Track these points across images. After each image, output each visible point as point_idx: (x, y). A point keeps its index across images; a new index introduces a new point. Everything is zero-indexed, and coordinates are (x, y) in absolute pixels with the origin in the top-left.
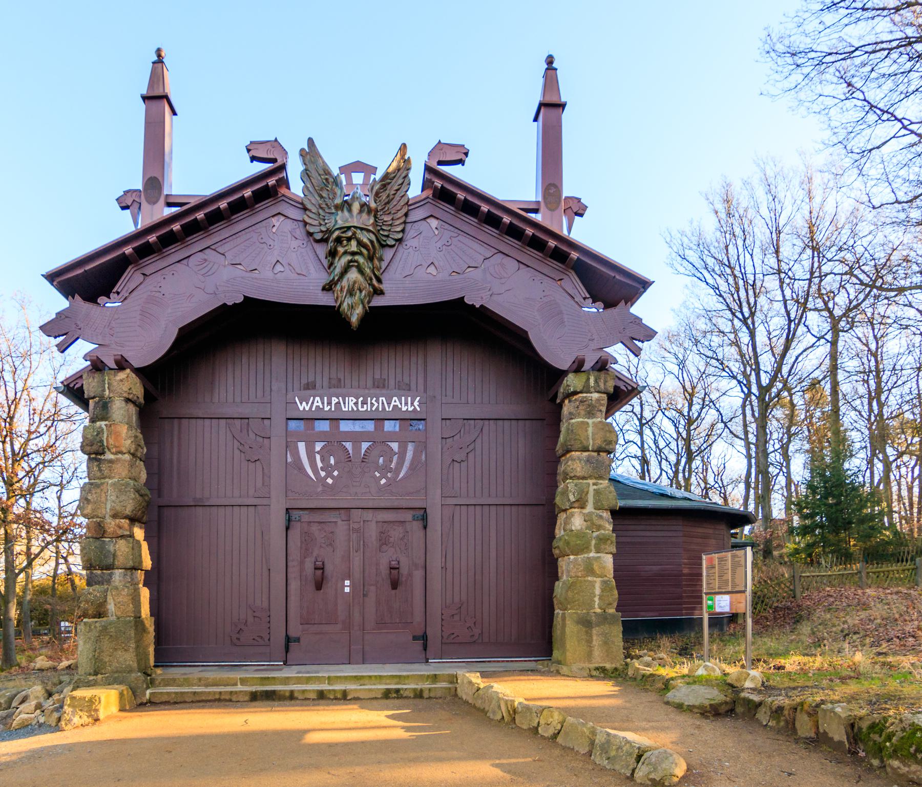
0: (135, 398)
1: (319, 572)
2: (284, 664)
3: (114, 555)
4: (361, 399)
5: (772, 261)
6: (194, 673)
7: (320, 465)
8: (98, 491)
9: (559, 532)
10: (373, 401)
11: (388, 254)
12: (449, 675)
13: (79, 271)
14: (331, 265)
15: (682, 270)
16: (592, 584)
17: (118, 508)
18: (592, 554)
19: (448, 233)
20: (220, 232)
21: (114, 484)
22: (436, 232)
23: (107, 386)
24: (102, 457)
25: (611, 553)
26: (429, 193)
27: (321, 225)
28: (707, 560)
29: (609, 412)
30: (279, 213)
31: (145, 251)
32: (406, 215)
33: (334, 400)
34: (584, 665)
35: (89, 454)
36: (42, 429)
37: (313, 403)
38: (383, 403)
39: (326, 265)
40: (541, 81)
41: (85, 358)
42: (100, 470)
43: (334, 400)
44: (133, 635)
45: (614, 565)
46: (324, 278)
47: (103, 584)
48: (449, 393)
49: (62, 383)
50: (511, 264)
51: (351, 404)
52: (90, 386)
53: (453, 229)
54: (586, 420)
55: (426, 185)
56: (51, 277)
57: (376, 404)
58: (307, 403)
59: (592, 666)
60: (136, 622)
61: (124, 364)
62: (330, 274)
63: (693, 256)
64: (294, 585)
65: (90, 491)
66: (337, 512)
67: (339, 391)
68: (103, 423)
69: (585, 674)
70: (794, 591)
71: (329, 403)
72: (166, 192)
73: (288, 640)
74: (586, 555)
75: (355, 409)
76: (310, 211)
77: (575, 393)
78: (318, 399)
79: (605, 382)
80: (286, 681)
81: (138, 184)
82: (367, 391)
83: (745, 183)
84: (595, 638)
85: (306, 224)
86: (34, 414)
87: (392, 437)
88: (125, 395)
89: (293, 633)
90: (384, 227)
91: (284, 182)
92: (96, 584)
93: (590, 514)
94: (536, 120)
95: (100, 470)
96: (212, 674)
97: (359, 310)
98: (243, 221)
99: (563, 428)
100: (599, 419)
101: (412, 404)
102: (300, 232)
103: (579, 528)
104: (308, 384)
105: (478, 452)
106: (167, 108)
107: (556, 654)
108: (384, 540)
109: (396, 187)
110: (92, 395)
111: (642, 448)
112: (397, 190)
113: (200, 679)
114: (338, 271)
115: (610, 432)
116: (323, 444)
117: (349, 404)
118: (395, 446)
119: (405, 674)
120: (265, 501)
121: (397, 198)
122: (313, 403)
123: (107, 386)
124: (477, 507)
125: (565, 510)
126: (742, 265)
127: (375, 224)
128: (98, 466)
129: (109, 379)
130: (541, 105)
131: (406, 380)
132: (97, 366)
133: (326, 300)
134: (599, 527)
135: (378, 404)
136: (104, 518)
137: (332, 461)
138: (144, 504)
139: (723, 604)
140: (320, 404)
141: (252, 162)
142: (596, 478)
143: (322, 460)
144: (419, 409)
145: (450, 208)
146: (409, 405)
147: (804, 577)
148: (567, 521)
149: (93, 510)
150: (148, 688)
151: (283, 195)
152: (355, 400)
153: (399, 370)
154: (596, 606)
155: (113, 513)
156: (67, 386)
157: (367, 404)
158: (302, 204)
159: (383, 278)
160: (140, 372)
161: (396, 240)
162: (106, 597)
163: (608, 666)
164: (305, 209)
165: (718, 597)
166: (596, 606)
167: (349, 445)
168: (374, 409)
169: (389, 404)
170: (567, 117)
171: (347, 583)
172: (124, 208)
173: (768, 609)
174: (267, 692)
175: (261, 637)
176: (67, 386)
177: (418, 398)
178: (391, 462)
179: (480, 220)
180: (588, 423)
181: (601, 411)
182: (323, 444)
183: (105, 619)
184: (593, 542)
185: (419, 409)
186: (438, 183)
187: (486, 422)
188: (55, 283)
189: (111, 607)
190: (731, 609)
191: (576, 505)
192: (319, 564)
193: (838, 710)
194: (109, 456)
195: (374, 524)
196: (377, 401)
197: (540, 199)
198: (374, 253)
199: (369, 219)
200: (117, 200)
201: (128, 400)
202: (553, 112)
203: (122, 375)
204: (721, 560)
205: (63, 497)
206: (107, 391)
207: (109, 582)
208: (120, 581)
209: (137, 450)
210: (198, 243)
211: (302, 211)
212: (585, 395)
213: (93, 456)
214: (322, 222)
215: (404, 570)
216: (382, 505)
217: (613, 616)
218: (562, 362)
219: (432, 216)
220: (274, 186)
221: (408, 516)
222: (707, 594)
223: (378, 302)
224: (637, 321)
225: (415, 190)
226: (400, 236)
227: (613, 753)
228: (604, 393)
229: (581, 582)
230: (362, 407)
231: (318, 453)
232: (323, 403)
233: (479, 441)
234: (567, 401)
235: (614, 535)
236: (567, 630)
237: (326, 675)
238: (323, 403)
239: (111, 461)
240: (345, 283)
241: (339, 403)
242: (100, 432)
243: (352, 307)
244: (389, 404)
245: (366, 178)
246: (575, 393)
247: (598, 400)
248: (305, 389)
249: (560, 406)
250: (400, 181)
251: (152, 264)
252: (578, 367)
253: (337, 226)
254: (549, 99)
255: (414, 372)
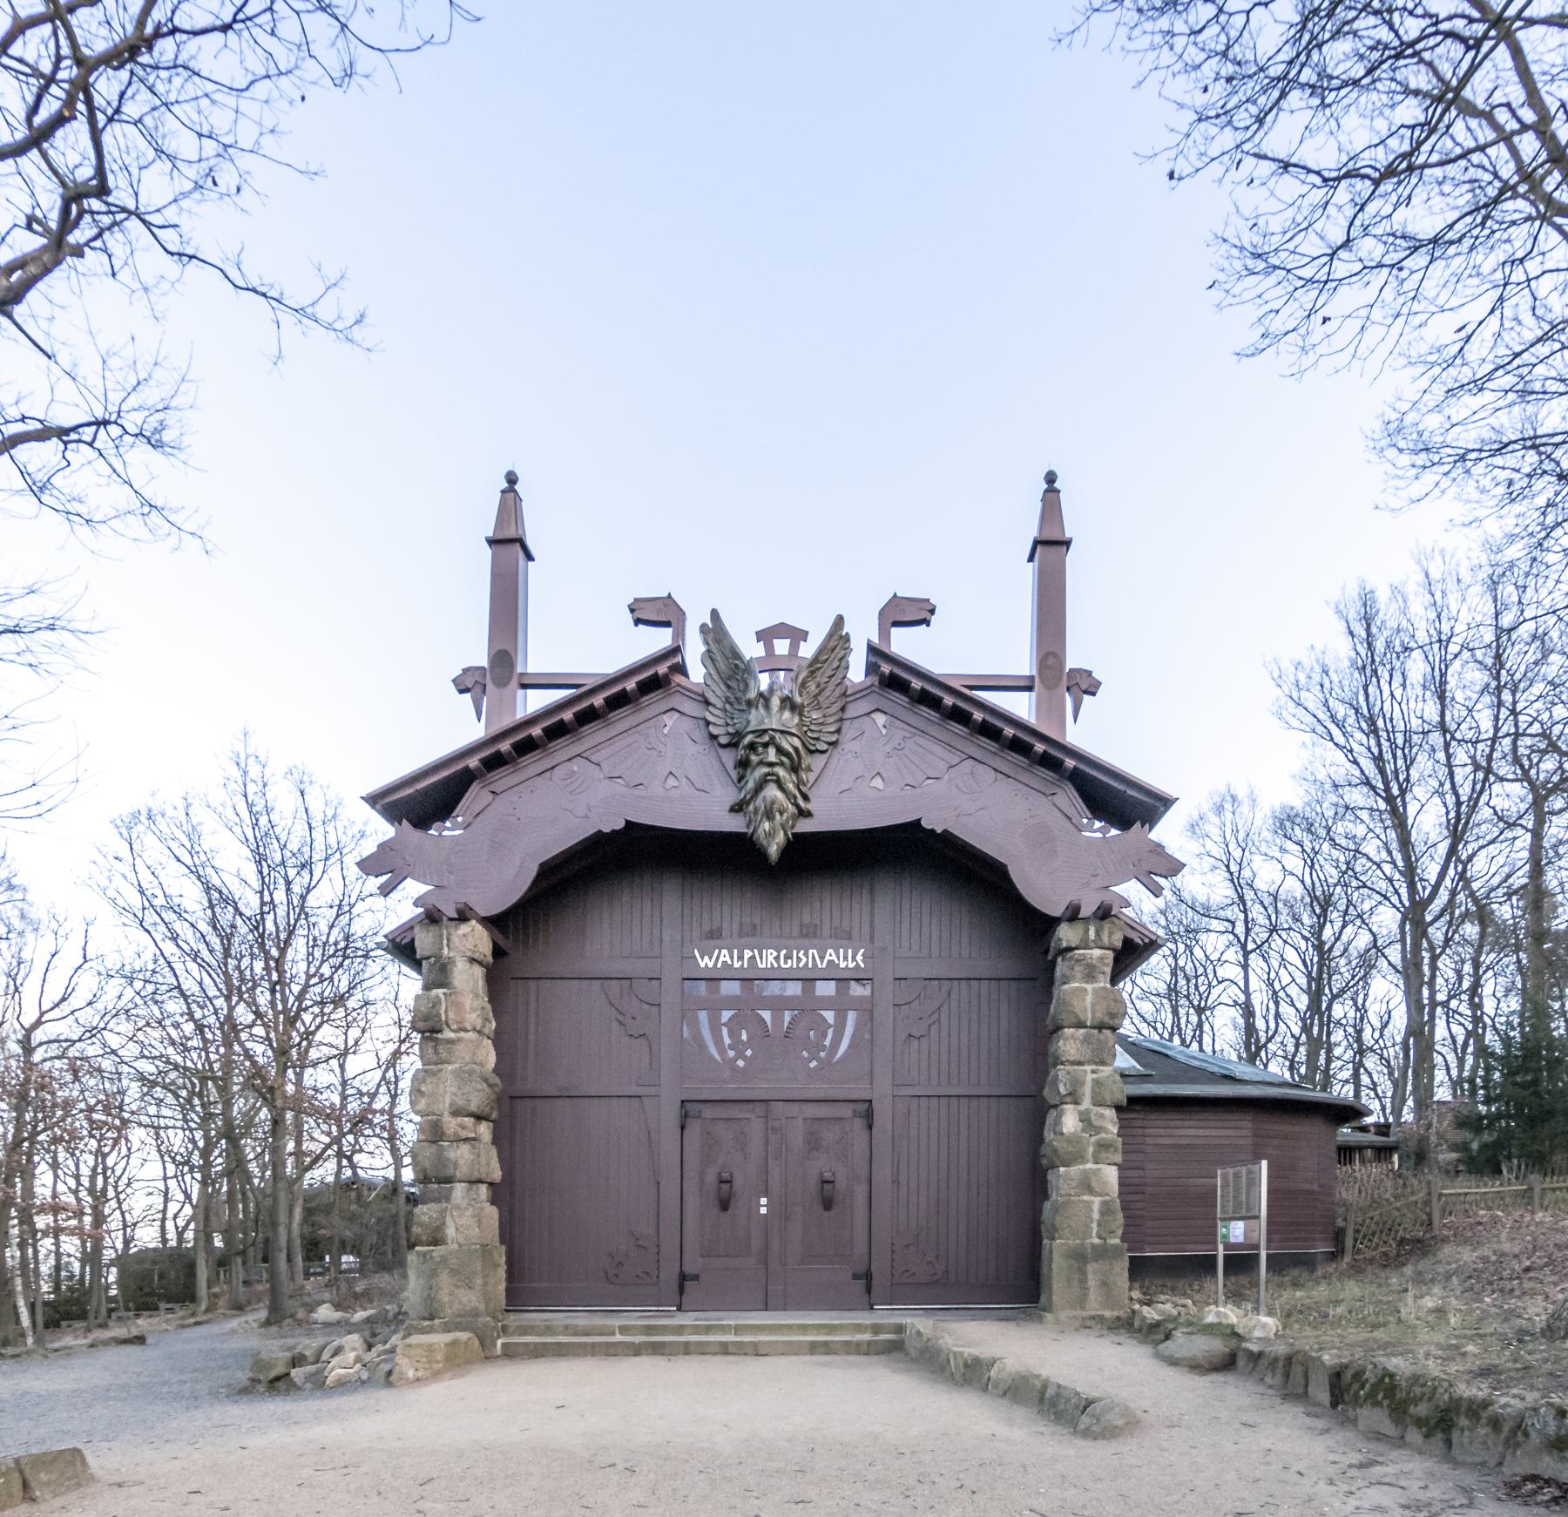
0: (482, 957)
1: (725, 1187)
2: (679, 1309)
3: (456, 1164)
4: (784, 952)
5: (1431, 710)
6: (559, 1319)
7: (727, 1041)
8: (435, 1080)
9: (1048, 1135)
10: (801, 955)
11: (817, 762)
12: (895, 1325)
13: (409, 791)
14: (741, 778)
15: (1295, 723)
16: (1089, 1205)
17: (461, 1102)
18: (1089, 1166)
19: (900, 733)
20: (593, 735)
21: (454, 1072)
22: (884, 731)
23: (445, 942)
24: (439, 1036)
25: (1115, 1164)
26: (875, 680)
27: (728, 725)
28: (1222, 1175)
29: (1115, 978)
30: (673, 709)
31: (495, 762)
32: (843, 709)
33: (747, 954)
34: (1075, 1313)
35: (422, 1032)
36: (326, 970)
37: (718, 957)
38: (813, 957)
39: (735, 777)
40: (1040, 504)
41: (416, 904)
42: (436, 1053)
43: (747, 954)
44: (479, 1268)
45: (1120, 1185)
46: (731, 796)
47: (440, 1202)
48: (905, 944)
49: (385, 936)
50: (985, 774)
51: (771, 958)
52: (424, 941)
53: (907, 727)
54: (1084, 985)
55: (871, 669)
56: (373, 800)
57: (804, 959)
58: (710, 958)
59: (1086, 1314)
60: (484, 1251)
61: (468, 914)
62: (740, 790)
63: (1312, 700)
64: (692, 1202)
65: (424, 1081)
66: (751, 1106)
67: (753, 940)
68: (440, 991)
69: (1077, 1324)
70: (1430, 1215)
71: (741, 958)
72: (519, 670)
73: (683, 1278)
74: (1081, 1167)
75: (776, 965)
76: (714, 706)
77: (1070, 949)
78: (725, 951)
79: (1111, 934)
80: (680, 1329)
81: (483, 661)
82: (792, 942)
83: (1395, 589)
84: (1090, 1277)
85: (708, 723)
86: (313, 947)
87: (827, 1003)
88: (469, 954)
89: (689, 1269)
90: (813, 728)
91: (681, 669)
92: (432, 1201)
93: (1088, 1111)
94: (1031, 559)
95: (436, 1053)
96: (582, 1320)
97: (780, 838)
98: (624, 719)
99: (1055, 992)
100: (1102, 985)
101: (854, 958)
102: (699, 734)
103: (1072, 1130)
104: (711, 931)
105: (944, 1022)
106: (521, 555)
107: (1043, 1299)
108: (813, 1144)
109: (830, 673)
110: (427, 954)
111: (1246, 992)
112: (830, 677)
113: (566, 1327)
114: (751, 785)
115: (1115, 1001)
116: (732, 1012)
117: (769, 959)
118: (829, 1016)
119: (836, 1322)
120: (653, 1091)
121: (831, 687)
122: (718, 957)
123: (445, 942)
124: (942, 1099)
125: (1056, 1106)
126: (1388, 716)
127: (801, 724)
128: (435, 1048)
129: (449, 934)
130: (1037, 543)
131: (846, 925)
132: (432, 917)
133: (735, 824)
134: (1099, 1130)
135: (806, 958)
136: (441, 1115)
137: (744, 1037)
138: (494, 1097)
139: (1237, 1231)
140: (728, 959)
141: (636, 625)
142: (1096, 1063)
143: (731, 1034)
144: (862, 965)
145: (903, 699)
146: (849, 959)
147: (1446, 1195)
148: (1058, 1122)
149: (428, 1105)
150: (498, 1337)
151: (679, 685)
152: (775, 954)
153: (836, 913)
154: (1094, 1234)
155: (454, 1108)
156: (392, 941)
157: (791, 958)
158: (703, 695)
159: (811, 796)
160: (492, 923)
161: (830, 744)
162: (444, 1218)
163: (1108, 1314)
164: (707, 703)
165: (1233, 1224)
166: (1094, 1234)
167: (766, 1015)
168: (801, 965)
169: (822, 958)
170: (1074, 561)
171: (764, 1201)
172: (461, 692)
173: (1391, 1242)
174: (654, 1343)
175: (647, 1274)
176: (392, 941)
177: (862, 951)
178: (824, 1036)
179: (942, 714)
180: (1086, 990)
181: (1104, 973)
182: (732, 1012)
183: (443, 1247)
184: (1091, 1149)
185: (862, 965)
186: (886, 668)
187: (956, 983)
188: (378, 806)
189: (450, 1232)
190: (1245, 1238)
191: (1068, 1099)
192: (725, 1176)
193: (1326, 1357)
194: (448, 1034)
195: (801, 1121)
196: (806, 955)
197: (1034, 673)
198: (800, 763)
199: (792, 719)
200: (454, 681)
201: (473, 960)
202: (1053, 551)
203: (464, 929)
204: (1237, 1176)
205: (347, 1066)
206: (446, 949)
207: (448, 1199)
208: (463, 1198)
209: (484, 1026)
210: (563, 749)
211: (702, 706)
212: (1082, 951)
213: (427, 1034)
214: (729, 721)
215: (841, 1184)
216: (811, 1096)
217: (1115, 1247)
218: (1053, 906)
219: (878, 710)
220: (666, 676)
221: (847, 1111)
222: (1222, 1220)
223: (804, 826)
224: (1158, 849)
225: (857, 672)
226: (833, 738)
227: (1062, 1407)
228: (1108, 949)
229: (1074, 1202)
230: (786, 963)
231: (725, 1025)
232: (732, 958)
233: (944, 1009)
234: (1059, 959)
235: (1120, 1139)
236: (1054, 1266)
237: (732, 1323)
238: (732, 958)
239: (450, 1041)
240: (759, 801)
241: (753, 957)
242: (436, 1003)
243: (770, 835)
244: (822, 958)
245: (794, 648)
246: (1070, 949)
247: (1101, 958)
248: (707, 938)
249: (1053, 963)
250: (836, 664)
251: (503, 778)
252: (1073, 915)
253: (750, 729)
254: (1048, 536)
255: (856, 920)
